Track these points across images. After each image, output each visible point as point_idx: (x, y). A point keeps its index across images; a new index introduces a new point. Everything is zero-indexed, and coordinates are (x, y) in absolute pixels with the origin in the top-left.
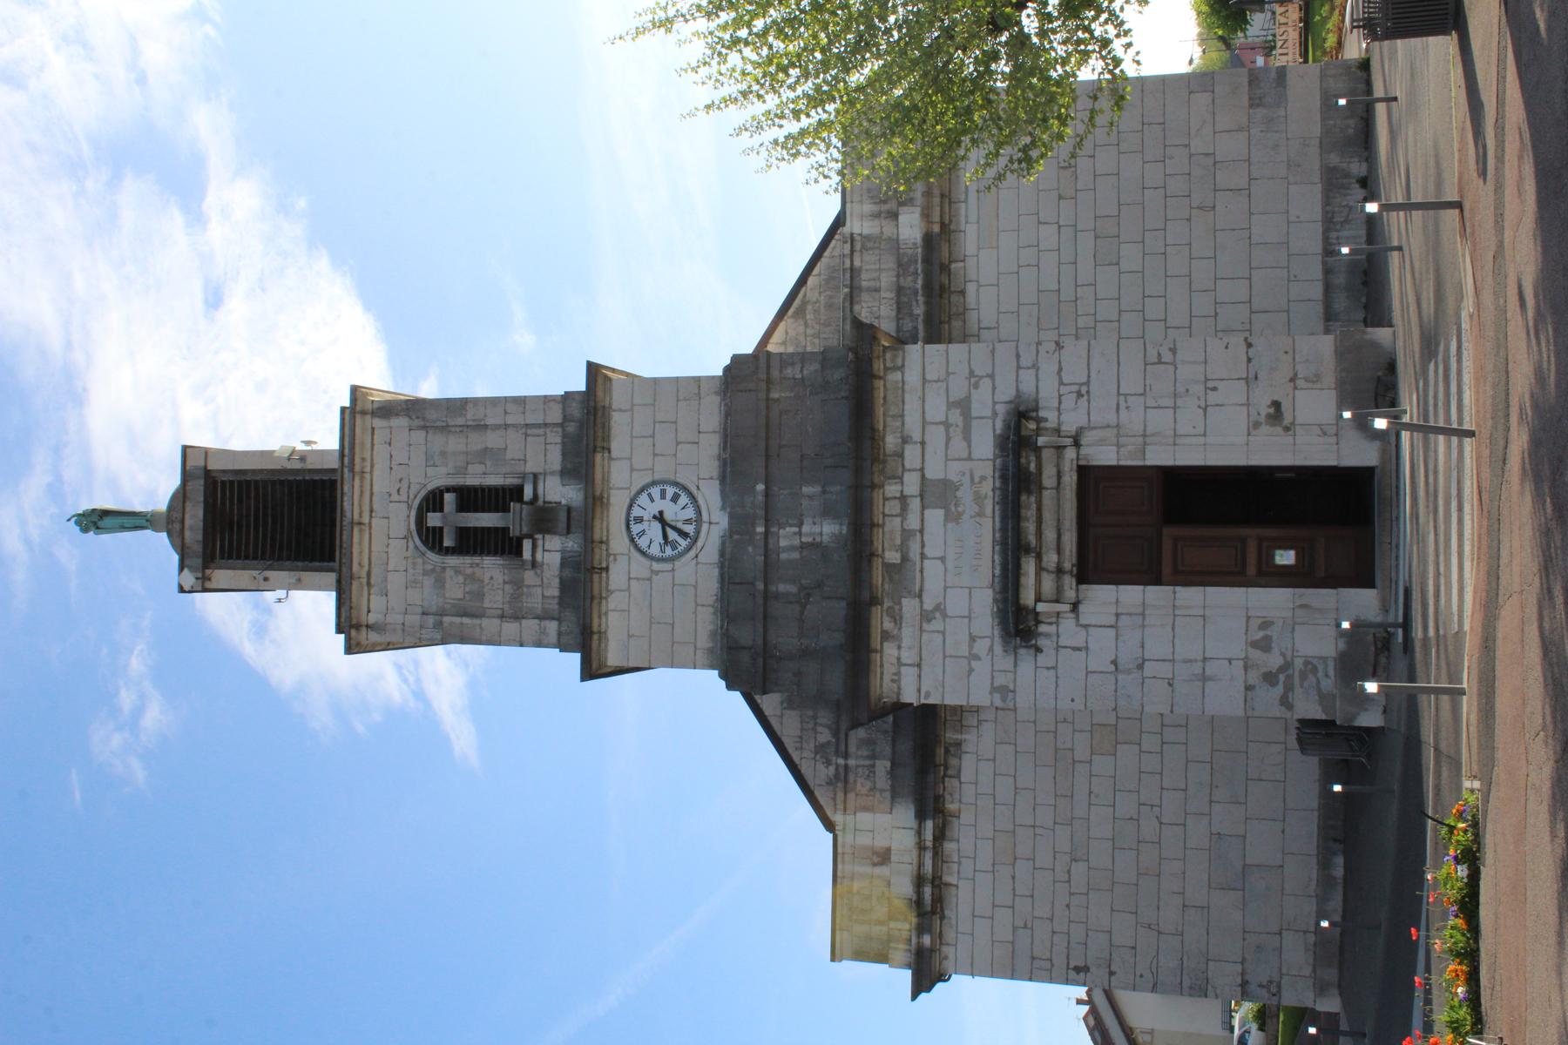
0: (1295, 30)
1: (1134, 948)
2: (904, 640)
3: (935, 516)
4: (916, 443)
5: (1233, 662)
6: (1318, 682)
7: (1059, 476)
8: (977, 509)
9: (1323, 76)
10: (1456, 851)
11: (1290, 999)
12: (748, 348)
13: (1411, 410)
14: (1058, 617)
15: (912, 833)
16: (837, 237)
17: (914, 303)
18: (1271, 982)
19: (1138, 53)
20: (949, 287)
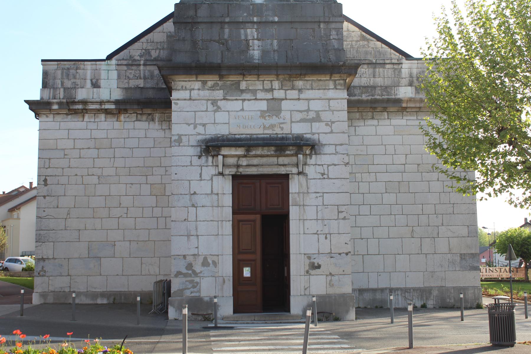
0: (498, 276)
1: (58, 207)
2: (202, 92)
3: (263, 106)
4: (299, 96)
5: (197, 249)
6: (188, 289)
7: (284, 165)
8: (267, 126)
9: (474, 287)
10: (109, 351)
11: (38, 281)
12: (345, 12)
13: (316, 328)
14: (216, 166)
15: (108, 98)
16: (401, 56)
17: (368, 95)
18: (45, 272)
19: (486, 199)
20: (375, 112)
